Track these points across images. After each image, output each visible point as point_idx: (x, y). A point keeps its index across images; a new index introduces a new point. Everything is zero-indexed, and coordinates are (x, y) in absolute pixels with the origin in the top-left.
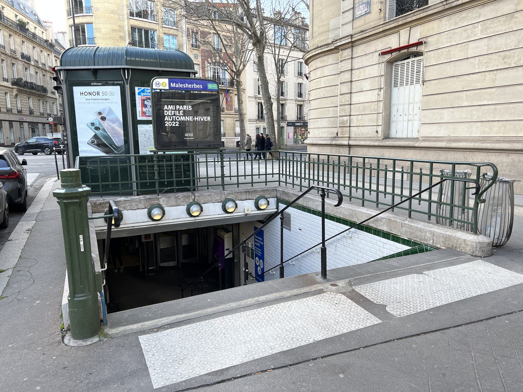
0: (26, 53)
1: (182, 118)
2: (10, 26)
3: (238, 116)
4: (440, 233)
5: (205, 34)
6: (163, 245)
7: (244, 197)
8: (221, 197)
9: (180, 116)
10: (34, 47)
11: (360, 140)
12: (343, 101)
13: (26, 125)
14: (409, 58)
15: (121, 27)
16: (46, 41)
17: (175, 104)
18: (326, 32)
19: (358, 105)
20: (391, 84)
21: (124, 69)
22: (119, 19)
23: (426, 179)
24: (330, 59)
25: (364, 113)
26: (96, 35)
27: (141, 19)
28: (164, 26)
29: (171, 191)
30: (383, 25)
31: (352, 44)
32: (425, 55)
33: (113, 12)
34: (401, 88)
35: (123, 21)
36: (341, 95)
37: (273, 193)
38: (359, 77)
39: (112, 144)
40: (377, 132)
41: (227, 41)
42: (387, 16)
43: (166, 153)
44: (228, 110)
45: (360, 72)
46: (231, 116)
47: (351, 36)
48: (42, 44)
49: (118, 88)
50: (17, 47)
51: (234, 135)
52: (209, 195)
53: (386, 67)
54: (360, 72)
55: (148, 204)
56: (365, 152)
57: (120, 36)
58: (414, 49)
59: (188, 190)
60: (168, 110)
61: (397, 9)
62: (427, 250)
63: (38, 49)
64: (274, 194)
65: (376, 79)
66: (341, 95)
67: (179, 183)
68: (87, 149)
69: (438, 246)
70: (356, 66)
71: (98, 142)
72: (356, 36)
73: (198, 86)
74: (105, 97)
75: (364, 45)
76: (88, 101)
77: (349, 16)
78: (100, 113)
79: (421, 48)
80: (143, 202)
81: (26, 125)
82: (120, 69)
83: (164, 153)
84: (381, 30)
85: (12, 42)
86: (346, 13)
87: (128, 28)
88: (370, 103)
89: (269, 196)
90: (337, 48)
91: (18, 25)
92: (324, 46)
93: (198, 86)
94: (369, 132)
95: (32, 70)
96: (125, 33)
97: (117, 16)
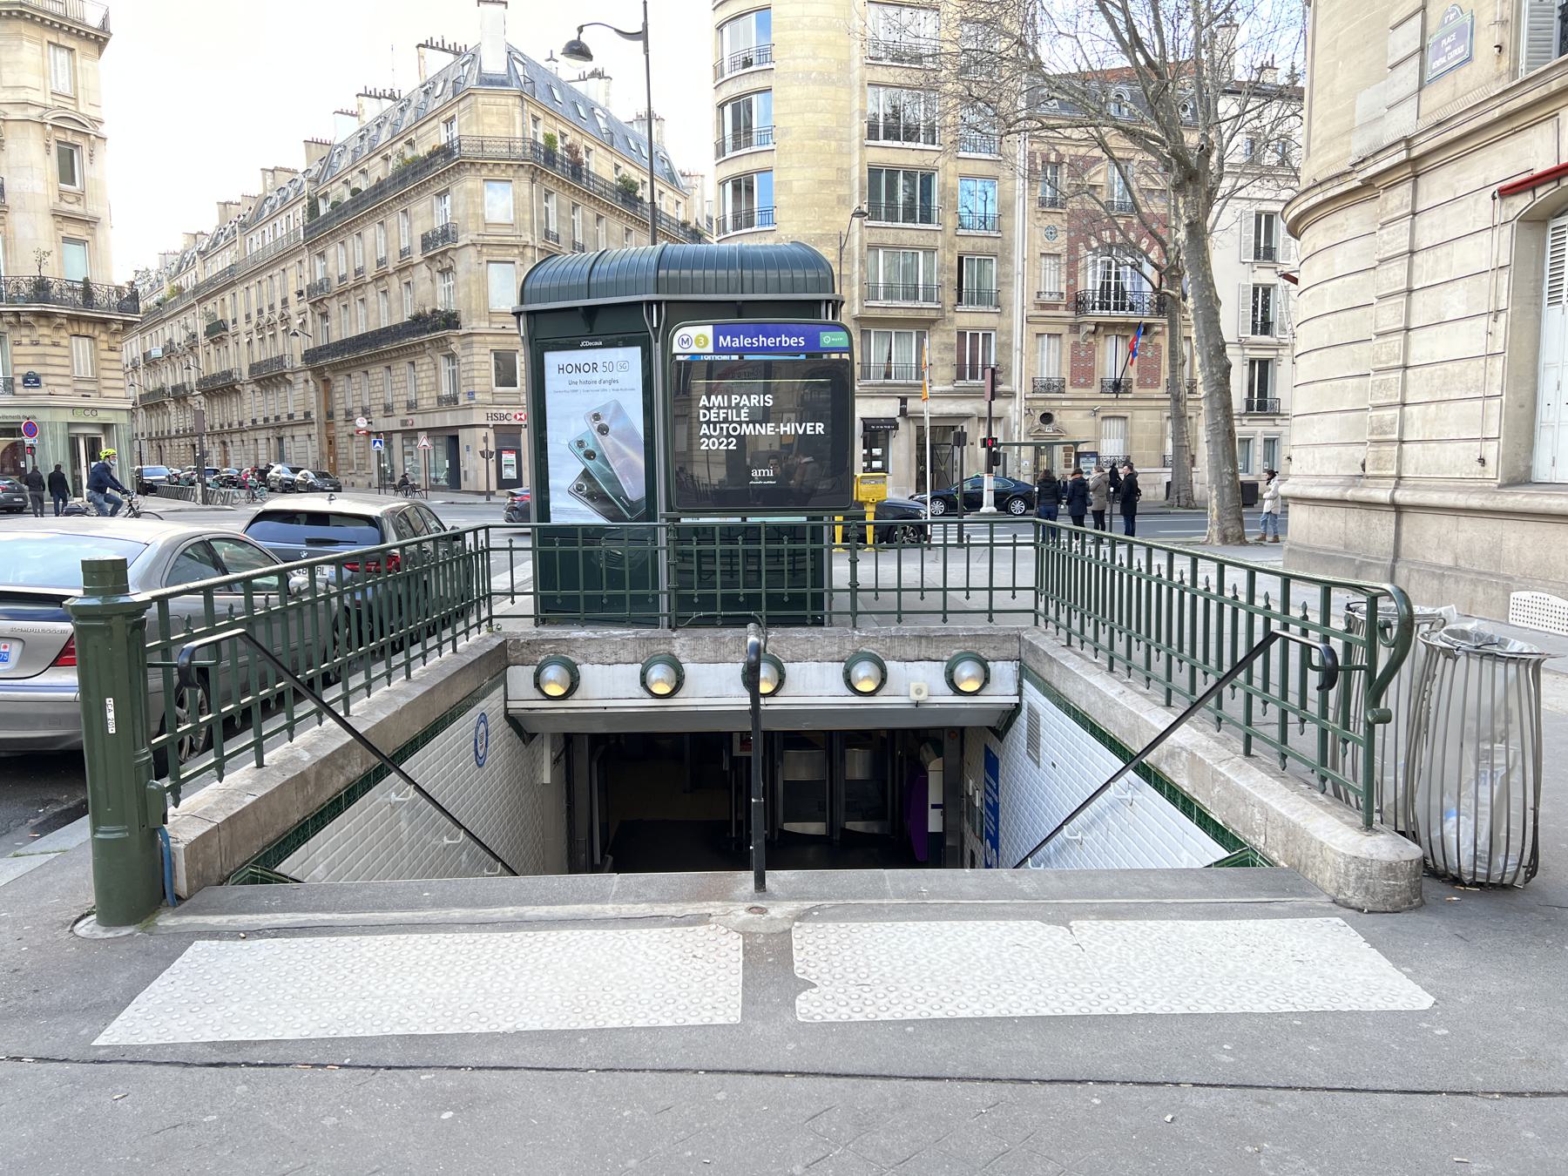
1: (747, 430)
2: (600, 194)
3: (1168, 403)
4: (1280, 814)
5: (1080, 167)
6: (799, 768)
7: (911, 651)
8: (841, 649)
9: (740, 423)
11: (1429, 489)
12: (1384, 358)
15: (844, 172)
16: (685, 225)
17: (729, 392)
18: (1344, 134)
19: (1427, 369)
20: (1539, 295)
21: (650, 303)
24: (1352, 222)
25: (1446, 397)
26: (780, 199)
27: (897, 144)
28: (962, 154)
29: (709, 622)
30: (1503, 99)
31: (1414, 168)
33: (825, 134)
35: (850, 153)
36: (1378, 335)
37: (1008, 645)
38: (1433, 277)
39: (620, 494)
40: (1482, 461)
41: (1153, 180)
42: (1522, 65)
43: (749, 520)
44: (1142, 385)
45: (1437, 261)
46: (1154, 403)
47: (1408, 142)
48: (673, 233)
49: (636, 351)
51: (1158, 461)
52: (807, 640)
53: (1518, 237)
54: (1437, 261)
55: (642, 653)
56: (1444, 531)
57: (839, 197)
59: (800, 622)
60: (709, 409)
62: (1254, 865)
64: (1012, 648)
65: (1485, 278)
66: (1378, 335)
67: (730, 601)
68: (569, 510)
69: (1275, 855)
70: (1424, 239)
71: (592, 489)
72: (1421, 139)
73: (793, 341)
74: (608, 376)
75: (1452, 168)
76: (574, 387)
77: (1408, 76)
78: (597, 417)
80: (631, 646)
82: (640, 303)
83: (744, 519)
84: (1497, 113)
85: (602, 234)
86: (1401, 67)
87: (861, 172)
88: (1464, 364)
89: (993, 654)
90: (1368, 184)
91: (619, 189)
92: (1330, 179)
93: (793, 341)
94: (1456, 460)
96: (851, 188)
97: (833, 144)
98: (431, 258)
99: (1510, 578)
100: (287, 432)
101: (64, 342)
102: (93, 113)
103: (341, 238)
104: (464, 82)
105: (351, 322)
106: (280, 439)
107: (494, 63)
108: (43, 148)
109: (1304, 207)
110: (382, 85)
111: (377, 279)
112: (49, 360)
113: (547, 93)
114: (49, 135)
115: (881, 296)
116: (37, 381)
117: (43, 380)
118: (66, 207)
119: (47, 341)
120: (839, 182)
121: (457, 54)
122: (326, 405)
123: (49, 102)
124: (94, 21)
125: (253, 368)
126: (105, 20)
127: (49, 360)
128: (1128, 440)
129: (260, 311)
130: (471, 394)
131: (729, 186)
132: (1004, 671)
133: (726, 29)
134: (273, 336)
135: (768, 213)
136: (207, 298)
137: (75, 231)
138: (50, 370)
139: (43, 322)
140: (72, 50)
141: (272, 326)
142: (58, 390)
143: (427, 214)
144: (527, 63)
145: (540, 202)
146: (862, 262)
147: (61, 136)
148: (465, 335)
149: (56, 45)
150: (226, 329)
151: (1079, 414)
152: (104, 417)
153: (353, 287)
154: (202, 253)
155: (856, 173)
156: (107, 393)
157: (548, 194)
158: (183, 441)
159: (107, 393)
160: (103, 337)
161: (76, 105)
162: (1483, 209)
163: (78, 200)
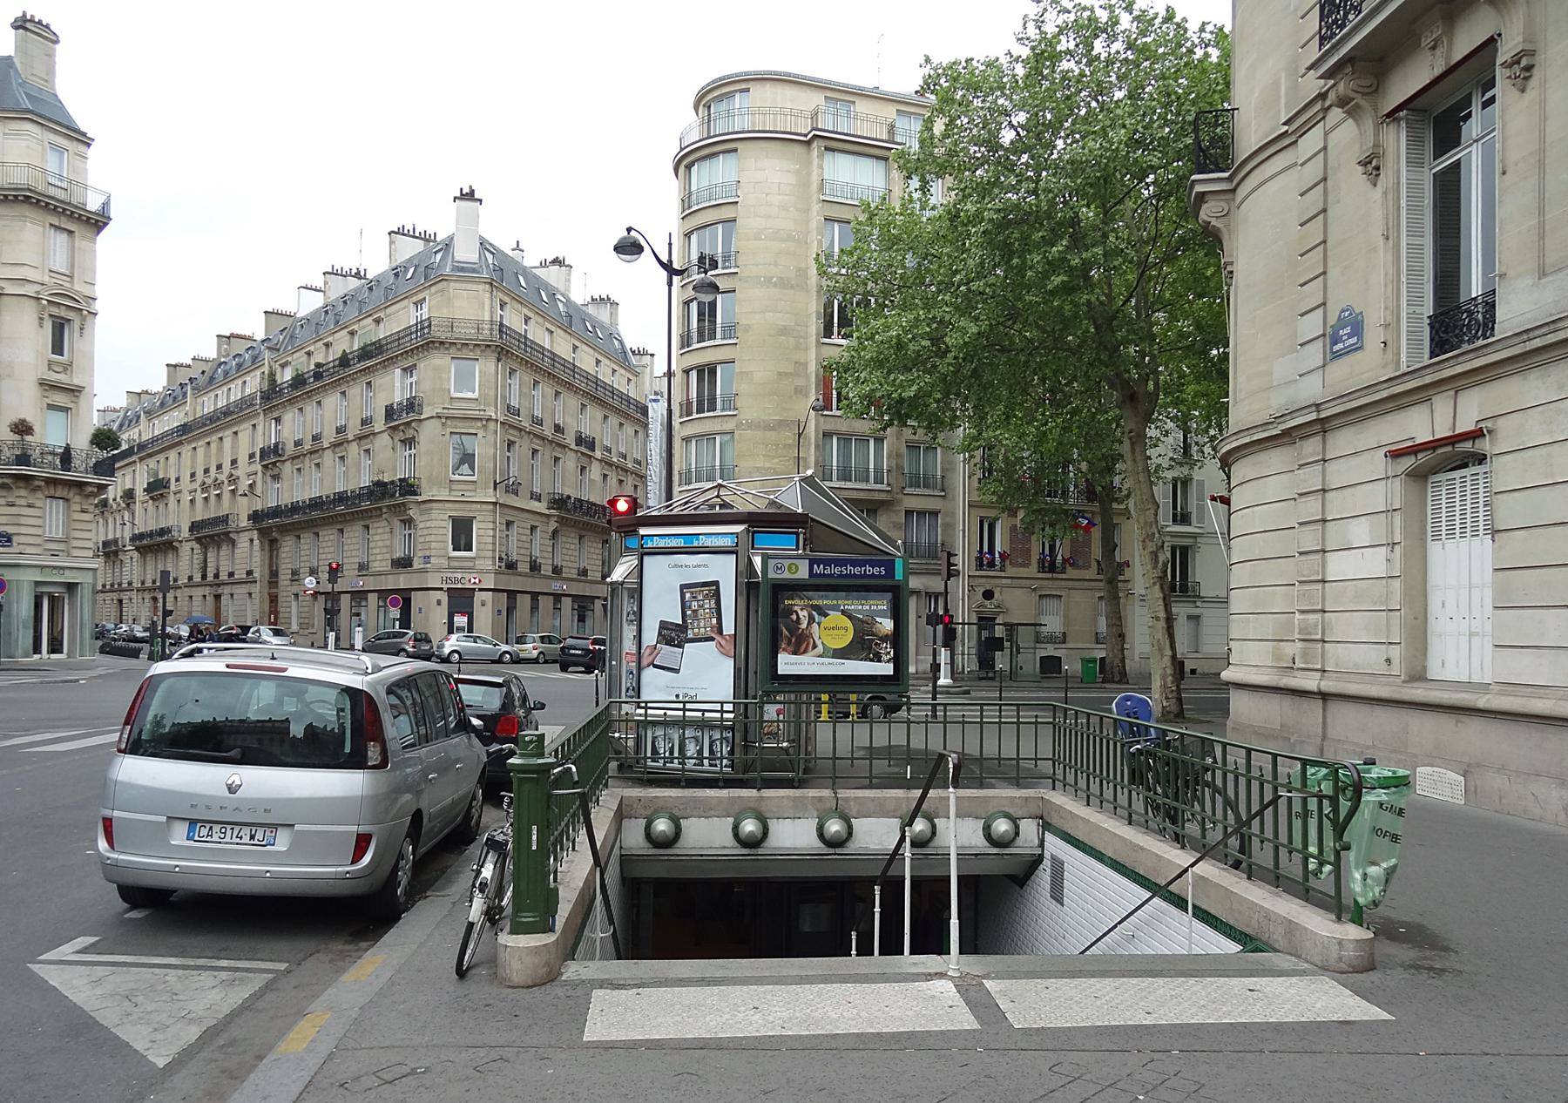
0: (586, 432)
10: (606, 417)
13: (567, 603)
14: (1465, 466)
22: (797, 347)
23: (1268, 788)
31: (1323, 426)
32: (1499, 463)
33: (784, 331)
34: (1450, 545)
35: (807, 349)
36: (1301, 554)
40: (1388, 661)
42: (1404, 359)
50: (568, 419)
58: (1467, 446)
61: (1432, 340)
63: (614, 420)
66: (1301, 554)
75: (1352, 429)
79: (1484, 446)
81: (567, 603)
84: (1385, 394)
90: (1286, 433)
95: (595, 471)
97: (792, 340)
98: (394, 428)
99: (1415, 756)
100: (226, 590)
101: (39, 503)
102: (86, 291)
103: (300, 405)
104: (428, 267)
105: (299, 487)
106: (218, 597)
107: (466, 252)
108: (36, 322)
109: (1234, 445)
110: (349, 264)
111: (335, 446)
112: (23, 521)
113: (513, 280)
114: (44, 308)
115: (835, 477)
116: (9, 540)
117: (15, 539)
118: (54, 377)
119: (23, 502)
120: (796, 374)
121: (427, 241)
122: (271, 565)
123: (46, 279)
124: (93, 204)
125: (194, 527)
126: (106, 205)
127: (23, 521)
128: (1067, 619)
129: (206, 471)
130: (427, 559)
131: (694, 374)
132: (1029, 829)
133: (694, 237)
135: (730, 402)
136: (150, 456)
137: (60, 399)
138: (23, 530)
139: (21, 484)
140: (71, 232)
141: (218, 485)
142: (29, 550)
143: (393, 387)
144: (496, 252)
145: (504, 378)
146: (817, 446)
147: (55, 311)
148: (424, 502)
149: (57, 228)
150: (167, 486)
151: (1018, 592)
152: (69, 577)
153: (311, 451)
154: (148, 413)
155: (812, 368)
156: (75, 553)
157: (512, 371)
158: (108, 596)
159: (75, 553)
160: (77, 499)
161: (72, 282)
162: (1377, 464)
163: (65, 369)
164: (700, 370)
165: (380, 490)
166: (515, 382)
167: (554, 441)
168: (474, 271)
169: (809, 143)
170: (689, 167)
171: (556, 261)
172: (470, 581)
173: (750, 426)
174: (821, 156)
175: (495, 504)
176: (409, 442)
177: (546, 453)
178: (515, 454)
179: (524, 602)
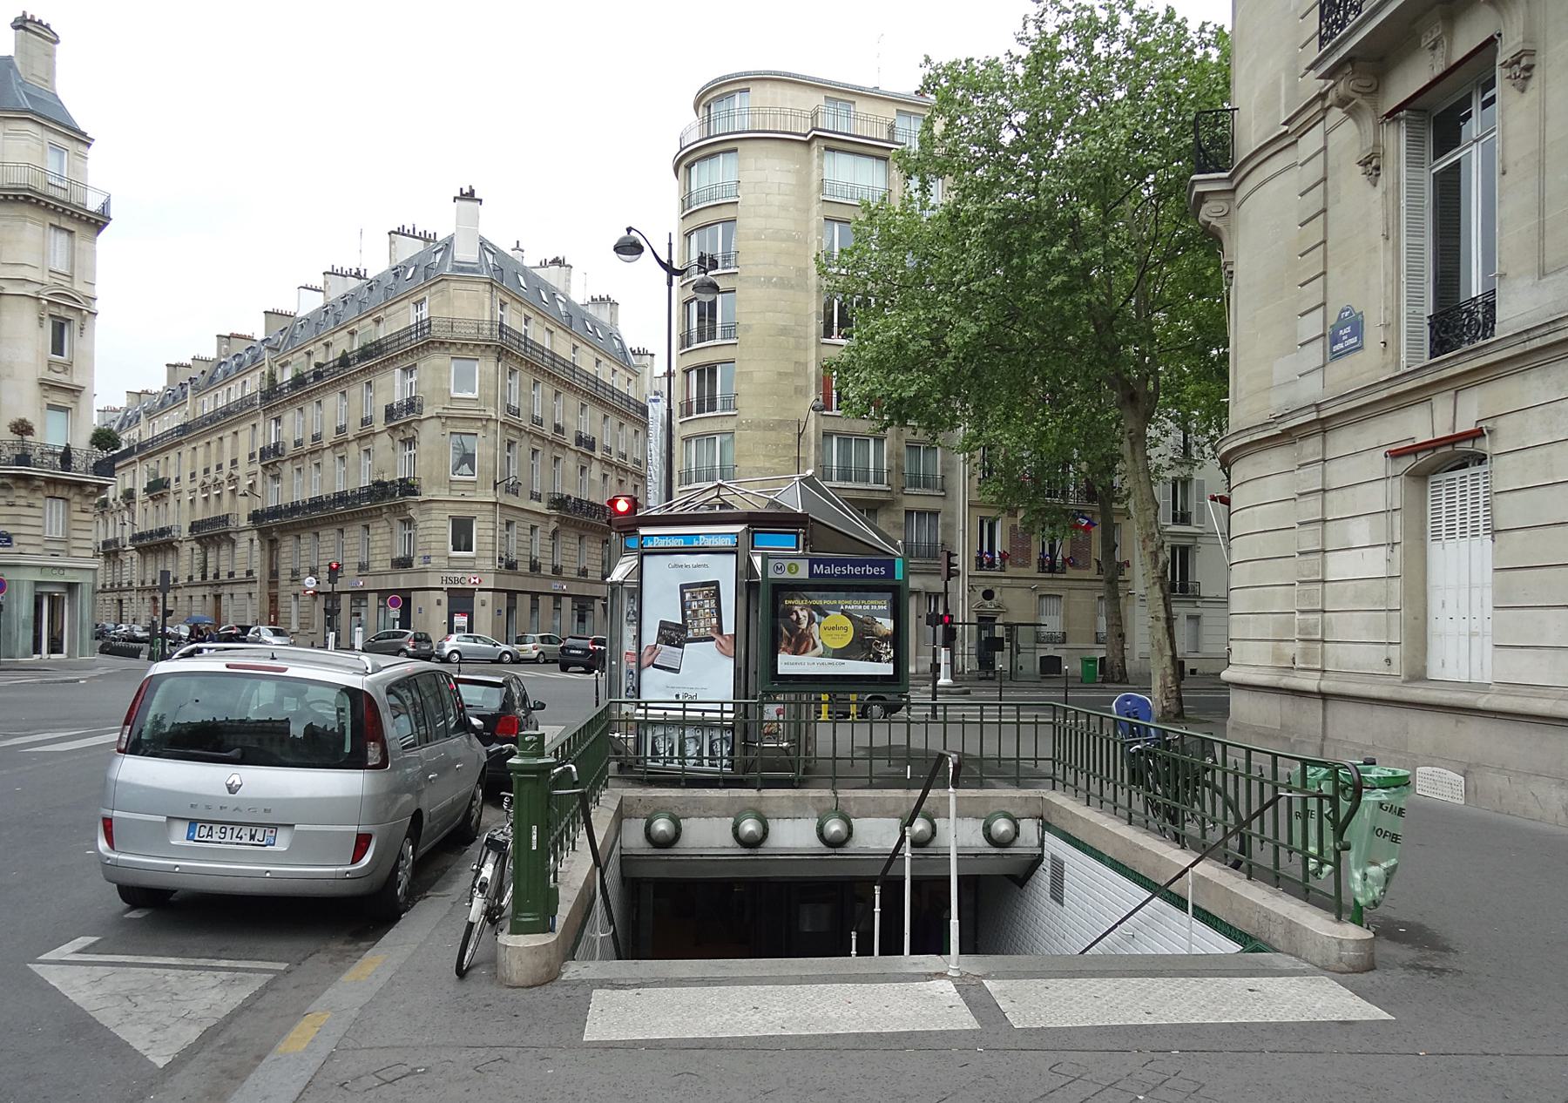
0: (586, 432)
10: (606, 417)
13: (567, 603)
14: (1465, 466)
22: (797, 347)
23: (1268, 788)
31: (1323, 426)
32: (1499, 463)
33: (784, 331)
34: (1450, 545)
35: (807, 349)
36: (1301, 554)
40: (1388, 661)
42: (1404, 359)
50: (568, 419)
58: (1467, 446)
61: (1432, 340)
63: (614, 420)
66: (1301, 554)
75: (1352, 429)
79: (1484, 446)
81: (567, 603)
84: (1385, 394)
90: (1286, 433)
95: (595, 471)
97: (792, 340)
98: (394, 428)
99: (1415, 756)
100: (226, 590)
101: (39, 503)
102: (86, 291)
103: (300, 405)
104: (428, 267)
105: (299, 487)
106: (218, 597)
107: (466, 252)
108: (36, 322)
109: (1234, 445)
110: (349, 264)
111: (335, 446)
112: (23, 521)
113: (513, 280)
114: (44, 308)
115: (835, 477)
116: (9, 540)
117: (15, 539)
118: (54, 377)
119: (23, 502)
120: (796, 374)
121: (427, 241)
122: (271, 565)
123: (46, 279)
124: (93, 204)
125: (194, 527)
126: (106, 205)
127: (23, 521)
128: (1067, 619)
129: (206, 471)
130: (427, 559)
131: (694, 374)
132: (1029, 829)
133: (694, 237)
134: (206, 499)
135: (730, 402)
136: (150, 456)
137: (60, 399)
138: (23, 530)
139: (21, 484)
140: (71, 232)
141: (218, 485)
142: (29, 550)
143: (393, 387)
144: (496, 252)
145: (504, 378)
146: (817, 446)
147: (55, 311)
148: (424, 502)
149: (57, 228)
150: (167, 486)
151: (1018, 592)
152: (69, 577)
153: (311, 451)
154: (148, 413)
155: (812, 368)
156: (75, 553)
157: (512, 371)
158: (108, 596)
159: (75, 553)
160: (77, 499)
161: (72, 282)
162: (1377, 464)
163: (65, 369)
164: (700, 370)
165: (380, 490)
166: (515, 382)
167: (554, 441)
168: (474, 271)
169: (809, 143)
170: (689, 167)
171: (556, 261)
172: (470, 581)
173: (750, 426)
174: (821, 156)
175: (495, 504)
176: (409, 442)
177: (546, 453)
178: (515, 454)
179: (524, 602)
